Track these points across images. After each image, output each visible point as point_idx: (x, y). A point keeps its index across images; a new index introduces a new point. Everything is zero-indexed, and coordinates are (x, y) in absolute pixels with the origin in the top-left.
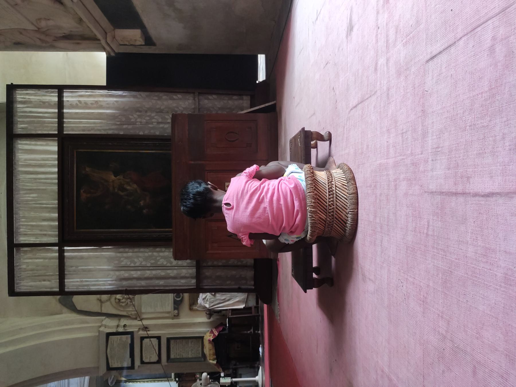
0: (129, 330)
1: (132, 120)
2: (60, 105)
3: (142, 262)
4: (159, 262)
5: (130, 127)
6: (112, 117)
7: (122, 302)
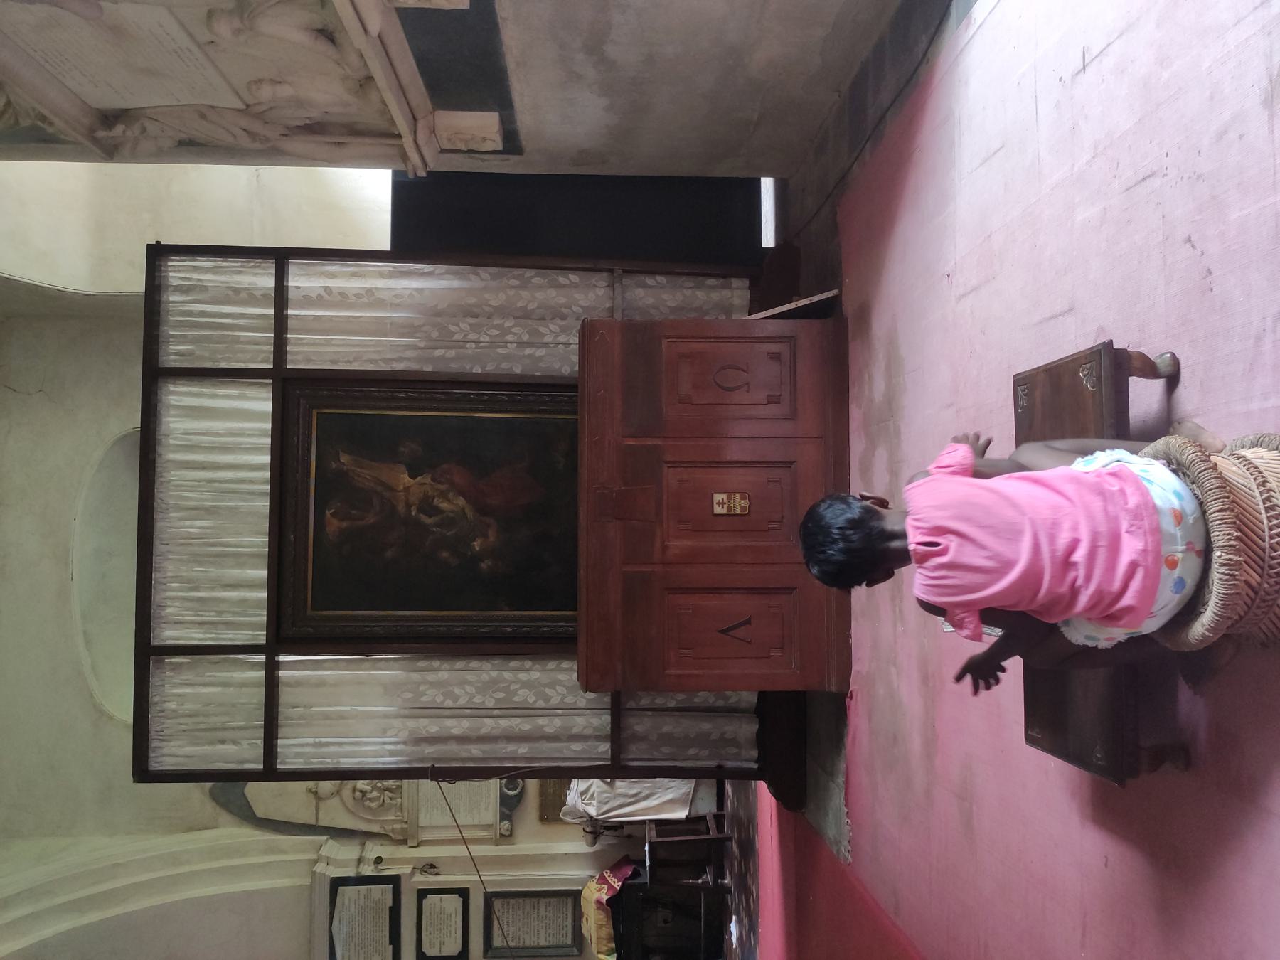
0: (389, 871)
1: (456, 337)
2: (281, 296)
3: (564, 697)
4: (545, 698)
5: (451, 353)
6: (408, 329)
7: (370, 800)
